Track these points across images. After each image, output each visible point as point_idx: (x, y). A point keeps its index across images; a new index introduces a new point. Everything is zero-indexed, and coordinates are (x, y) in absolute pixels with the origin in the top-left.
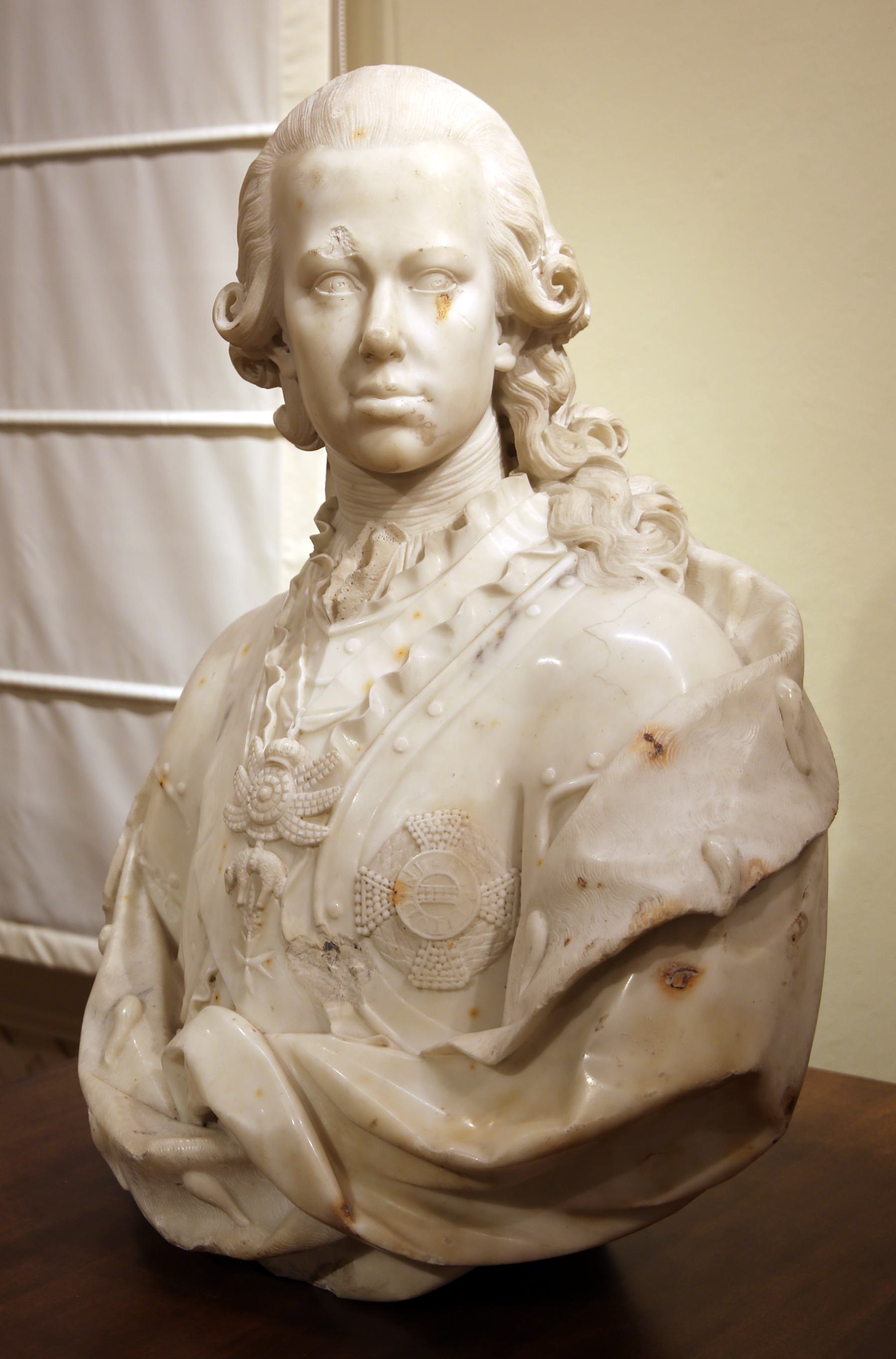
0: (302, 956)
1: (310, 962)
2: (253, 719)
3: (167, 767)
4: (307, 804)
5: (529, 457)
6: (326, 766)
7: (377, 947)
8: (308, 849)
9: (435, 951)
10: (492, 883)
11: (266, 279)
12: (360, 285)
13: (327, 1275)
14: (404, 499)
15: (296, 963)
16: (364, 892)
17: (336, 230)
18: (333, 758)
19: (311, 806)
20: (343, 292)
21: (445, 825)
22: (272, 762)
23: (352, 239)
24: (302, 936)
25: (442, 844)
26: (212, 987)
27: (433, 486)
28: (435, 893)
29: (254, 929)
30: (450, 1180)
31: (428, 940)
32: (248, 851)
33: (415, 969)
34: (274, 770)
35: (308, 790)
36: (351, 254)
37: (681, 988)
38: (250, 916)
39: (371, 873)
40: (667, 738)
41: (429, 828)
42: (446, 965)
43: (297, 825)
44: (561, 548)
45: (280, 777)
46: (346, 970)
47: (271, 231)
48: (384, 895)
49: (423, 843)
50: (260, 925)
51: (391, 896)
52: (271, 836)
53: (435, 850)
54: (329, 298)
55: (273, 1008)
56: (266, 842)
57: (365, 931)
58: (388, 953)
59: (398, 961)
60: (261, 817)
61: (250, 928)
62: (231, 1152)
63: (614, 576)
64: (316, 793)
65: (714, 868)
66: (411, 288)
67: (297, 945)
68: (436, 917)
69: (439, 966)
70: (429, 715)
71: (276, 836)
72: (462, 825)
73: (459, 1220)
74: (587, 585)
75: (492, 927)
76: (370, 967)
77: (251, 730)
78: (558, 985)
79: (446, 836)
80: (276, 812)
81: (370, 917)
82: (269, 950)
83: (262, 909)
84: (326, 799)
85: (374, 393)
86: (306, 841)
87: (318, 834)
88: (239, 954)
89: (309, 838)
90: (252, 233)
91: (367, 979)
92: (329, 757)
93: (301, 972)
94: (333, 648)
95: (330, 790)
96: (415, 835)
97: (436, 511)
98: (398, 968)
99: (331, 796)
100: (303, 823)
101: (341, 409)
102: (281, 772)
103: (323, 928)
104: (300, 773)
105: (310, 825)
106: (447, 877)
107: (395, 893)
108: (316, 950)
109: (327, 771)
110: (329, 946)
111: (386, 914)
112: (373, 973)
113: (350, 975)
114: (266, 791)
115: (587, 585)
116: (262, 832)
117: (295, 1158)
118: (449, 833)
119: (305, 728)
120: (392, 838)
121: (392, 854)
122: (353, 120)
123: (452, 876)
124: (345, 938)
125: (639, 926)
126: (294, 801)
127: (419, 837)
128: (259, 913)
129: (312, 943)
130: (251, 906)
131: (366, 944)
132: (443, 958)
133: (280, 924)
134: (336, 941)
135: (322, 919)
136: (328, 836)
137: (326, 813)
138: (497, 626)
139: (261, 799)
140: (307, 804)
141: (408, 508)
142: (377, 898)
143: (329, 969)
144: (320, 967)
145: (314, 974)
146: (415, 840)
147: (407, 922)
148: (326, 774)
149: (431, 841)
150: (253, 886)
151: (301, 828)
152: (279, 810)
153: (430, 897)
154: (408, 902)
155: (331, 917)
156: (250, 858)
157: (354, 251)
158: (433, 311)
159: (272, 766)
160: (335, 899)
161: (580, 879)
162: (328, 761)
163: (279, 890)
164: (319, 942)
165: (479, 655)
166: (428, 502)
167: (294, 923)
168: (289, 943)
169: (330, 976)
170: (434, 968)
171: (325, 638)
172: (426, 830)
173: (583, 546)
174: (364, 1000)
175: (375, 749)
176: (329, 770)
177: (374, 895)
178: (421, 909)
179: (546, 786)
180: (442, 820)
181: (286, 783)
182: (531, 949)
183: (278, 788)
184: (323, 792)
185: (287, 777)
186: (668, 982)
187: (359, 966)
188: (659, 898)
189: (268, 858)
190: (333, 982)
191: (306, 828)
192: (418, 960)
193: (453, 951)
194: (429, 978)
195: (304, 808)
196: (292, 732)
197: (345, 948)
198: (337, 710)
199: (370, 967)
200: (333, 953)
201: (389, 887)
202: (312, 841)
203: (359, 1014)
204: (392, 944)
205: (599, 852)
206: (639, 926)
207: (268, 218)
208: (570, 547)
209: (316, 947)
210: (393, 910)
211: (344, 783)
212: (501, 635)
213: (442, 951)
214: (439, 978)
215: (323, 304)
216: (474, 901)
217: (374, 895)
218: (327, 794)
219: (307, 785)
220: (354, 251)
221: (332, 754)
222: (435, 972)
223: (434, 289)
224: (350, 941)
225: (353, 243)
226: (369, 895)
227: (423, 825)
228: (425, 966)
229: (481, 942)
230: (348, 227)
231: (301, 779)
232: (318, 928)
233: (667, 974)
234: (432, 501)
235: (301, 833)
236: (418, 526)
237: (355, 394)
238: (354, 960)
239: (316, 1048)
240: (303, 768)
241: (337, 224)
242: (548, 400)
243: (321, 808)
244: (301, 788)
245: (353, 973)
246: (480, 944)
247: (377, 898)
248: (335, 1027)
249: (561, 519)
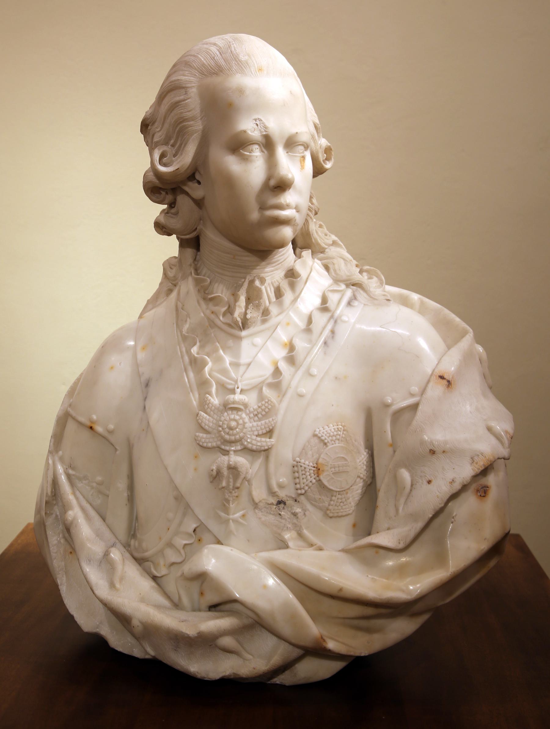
0: (263, 511)
1: (267, 513)
2: (190, 386)
3: (95, 417)
4: (259, 428)
5: (312, 241)
6: (266, 407)
7: (308, 499)
8: (263, 452)
9: (340, 496)
10: (361, 458)
11: (197, 145)
12: (264, 150)
13: (278, 675)
14: (264, 263)
15: (260, 514)
16: (300, 471)
17: (256, 120)
18: (270, 402)
19: (261, 429)
20: (257, 154)
21: (336, 431)
22: (231, 408)
23: (265, 125)
24: (263, 499)
25: (337, 441)
26: (195, 534)
27: (276, 257)
28: (339, 467)
29: (233, 499)
30: (370, 611)
31: (336, 492)
32: (226, 458)
33: (330, 507)
34: (235, 412)
35: (257, 421)
36: (264, 133)
37: (484, 496)
38: (231, 492)
39: (303, 461)
40: (451, 377)
41: (329, 434)
42: (345, 503)
43: (256, 440)
44: (343, 287)
45: (240, 416)
46: (289, 513)
47: (201, 119)
48: (312, 471)
49: (328, 442)
50: (237, 497)
51: (316, 472)
52: (239, 448)
53: (335, 445)
54: (250, 156)
55: (248, 541)
56: (235, 451)
57: (303, 491)
58: (316, 501)
59: (321, 505)
60: (233, 438)
61: (231, 499)
62: (246, 621)
63: (376, 299)
64: (263, 422)
65: (498, 437)
66: (287, 152)
67: (261, 505)
68: (340, 479)
69: (342, 504)
70: (311, 375)
71: (242, 447)
72: (344, 430)
73: (369, 630)
74: (364, 305)
75: (362, 480)
76: (305, 510)
77: (192, 391)
78: (440, 504)
79: (338, 437)
80: (241, 434)
81: (305, 484)
82: (243, 509)
83: (238, 488)
84: (269, 424)
85: (280, 207)
86: (263, 448)
87: (269, 444)
88: (222, 514)
89: (264, 446)
90: (187, 119)
91: (304, 517)
92: (268, 402)
93: (263, 518)
94: (245, 344)
95: (271, 419)
96: (323, 438)
97: (277, 269)
98: (320, 509)
99: (272, 423)
100: (259, 439)
101: (255, 215)
102: (240, 413)
103: (277, 493)
104: (250, 412)
105: (263, 439)
106: (343, 457)
107: (318, 470)
108: (271, 506)
109: (267, 410)
110: (279, 502)
111: (314, 481)
112: (307, 513)
113: (292, 516)
114: (233, 424)
115: (364, 305)
116: (233, 447)
117: (293, 617)
118: (339, 435)
119: (245, 388)
120: (309, 441)
121: (311, 450)
122: (254, 61)
123: (346, 457)
124: (290, 497)
125: (478, 469)
126: (251, 427)
127: (325, 439)
128: (236, 490)
129: (270, 502)
130: (231, 487)
131: (302, 498)
132: (344, 500)
133: (250, 494)
134: (284, 499)
135: (276, 489)
136: (273, 445)
137: (270, 433)
138: (329, 327)
139: (231, 428)
140: (259, 428)
141: (265, 268)
142: (308, 474)
143: (280, 514)
144: (274, 514)
145: (271, 518)
146: (322, 441)
147: (326, 483)
148: (265, 411)
149: (331, 441)
150: (231, 476)
151: (258, 441)
152: (244, 433)
153: (337, 469)
154: (325, 473)
155: (281, 486)
156: (229, 461)
157: (266, 131)
158: (298, 164)
159: (232, 410)
160: (281, 477)
161: (431, 450)
162: (266, 405)
163: (249, 477)
164: (274, 501)
165: (325, 343)
166: (274, 265)
167: (259, 493)
168: (257, 504)
169: (281, 518)
170: (340, 505)
171: (240, 338)
172: (328, 435)
173: (353, 285)
174: (303, 527)
175: (288, 396)
176: (269, 409)
177: (306, 472)
178: (333, 476)
179: (387, 406)
180: (334, 429)
181: (244, 418)
182: (404, 488)
183: (241, 422)
184: (267, 421)
185: (244, 415)
186: (479, 494)
187: (298, 510)
188: (482, 454)
189: (240, 460)
190: (283, 521)
191: (261, 441)
192: (332, 502)
193: (348, 495)
194: (338, 511)
195: (257, 430)
196: (238, 391)
197: (289, 502)
198: (261, 376)
199: (305, 510)
200: (282, 505)
201: (314, 467)
202: (266, 448)
203: (300, 535)
204: (317, 496)
205: (437, 435)
206: (478, 469)
207: (199, 111)
208: (347, 286)
209: (272, 504)
210: (317, 479)
211: (276, 415)
212: (333, 332)
213: (343, 496)
214: (342, 510)
215: (246, 159)
216: (356, 468)
217: (306, 472)
218: (269, 421)
219: (256, 418)
220: (266, 131)
221: (269, 400)
222: (340, 507)
223: (299, 154)
224: (293, 498)
225: (266, 127)
226: (303, 472)
227: (326, 433)
228: (336, 505)
229: (358, 489)
230: (262, 119)
231: (252, 415)
232: (272, 493)
233: (478, 491)
234: (276, 263)
235: (259, 444)
236: (269, 277)
237: (263, 207)
238: (295, 508)
239: (290, 558)
240: (252, 409)
241: (256, 117)
242: (314, 212)
243: (268, 430)
244: (252, 420)
245: (295, 515)
246: (357, 490)
247: (308, 474)
248: (291, 544)
249: (338, 272)
